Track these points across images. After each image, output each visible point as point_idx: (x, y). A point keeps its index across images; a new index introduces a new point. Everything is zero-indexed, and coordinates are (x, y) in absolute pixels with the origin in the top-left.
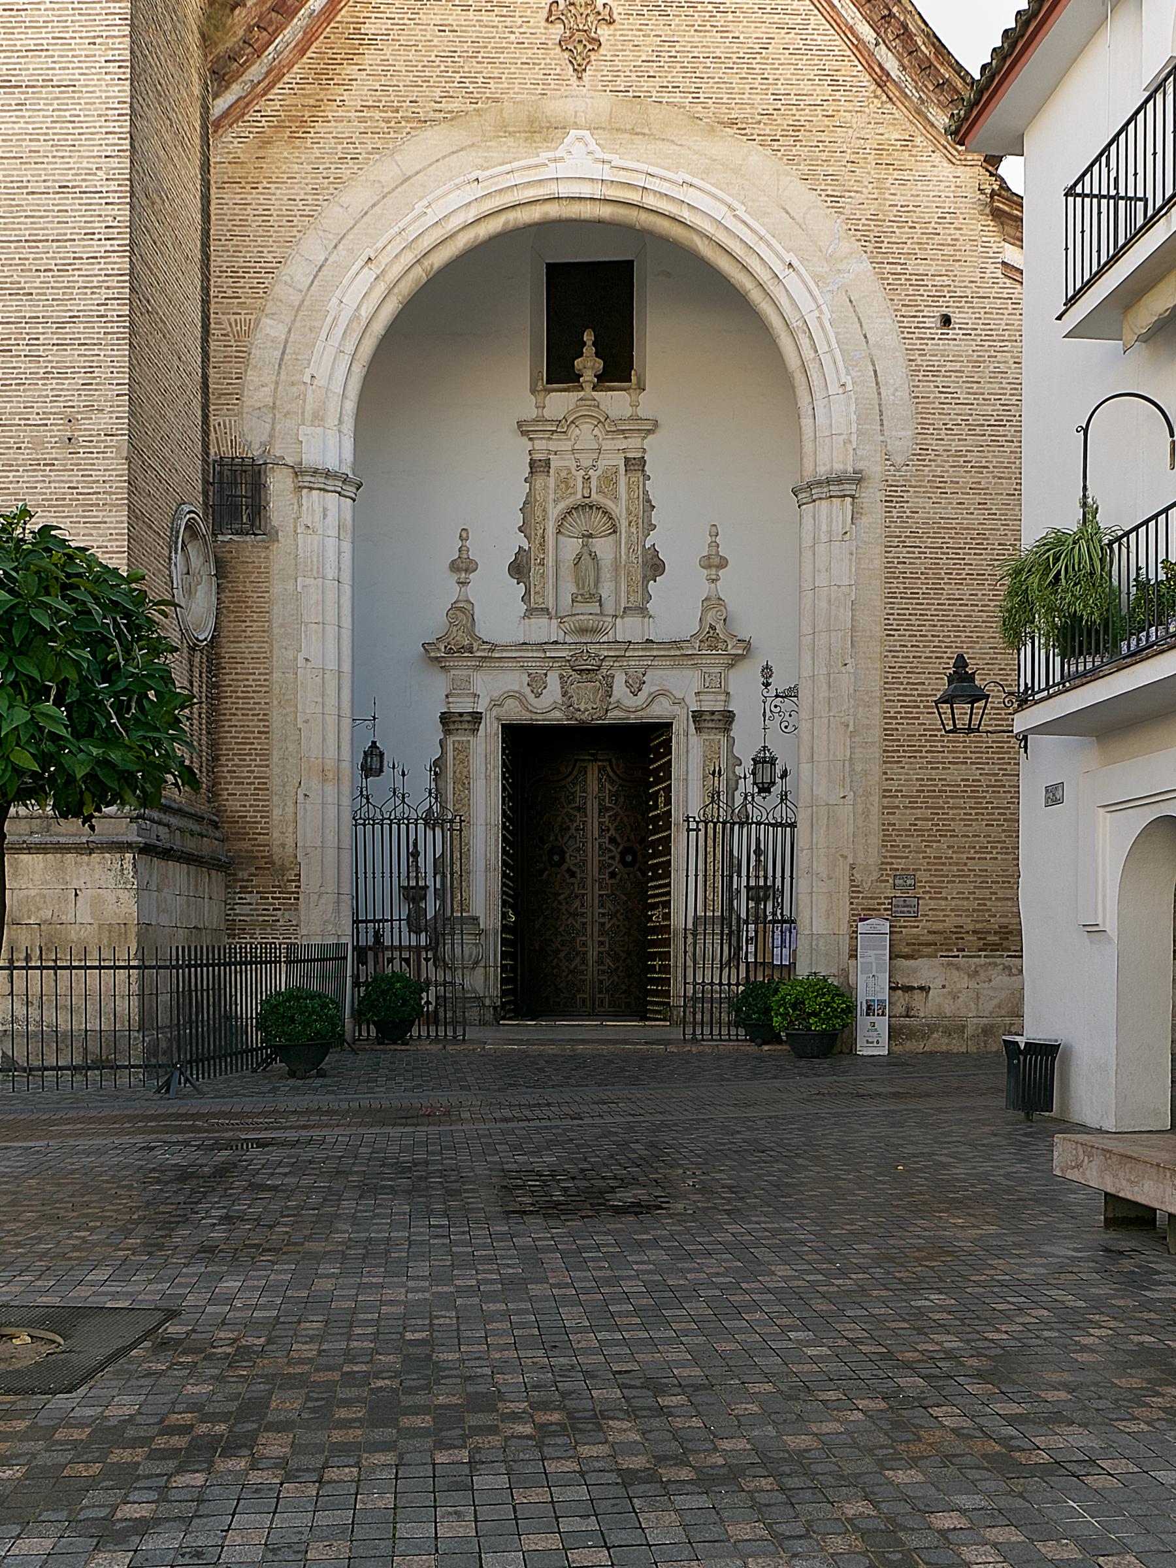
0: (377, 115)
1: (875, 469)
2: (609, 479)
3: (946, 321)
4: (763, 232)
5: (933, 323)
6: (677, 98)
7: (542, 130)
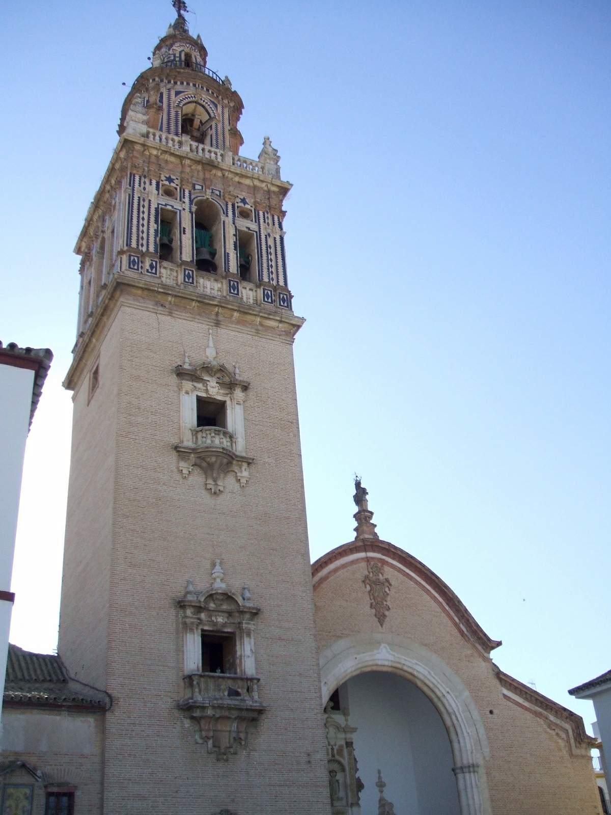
0: (324, 633)
1: (481, 762)
2: (340, 752)
3: (491, 712)
4: (439, 681)
5: (488, 713)
6: (409, 636)
7: (374, 644)
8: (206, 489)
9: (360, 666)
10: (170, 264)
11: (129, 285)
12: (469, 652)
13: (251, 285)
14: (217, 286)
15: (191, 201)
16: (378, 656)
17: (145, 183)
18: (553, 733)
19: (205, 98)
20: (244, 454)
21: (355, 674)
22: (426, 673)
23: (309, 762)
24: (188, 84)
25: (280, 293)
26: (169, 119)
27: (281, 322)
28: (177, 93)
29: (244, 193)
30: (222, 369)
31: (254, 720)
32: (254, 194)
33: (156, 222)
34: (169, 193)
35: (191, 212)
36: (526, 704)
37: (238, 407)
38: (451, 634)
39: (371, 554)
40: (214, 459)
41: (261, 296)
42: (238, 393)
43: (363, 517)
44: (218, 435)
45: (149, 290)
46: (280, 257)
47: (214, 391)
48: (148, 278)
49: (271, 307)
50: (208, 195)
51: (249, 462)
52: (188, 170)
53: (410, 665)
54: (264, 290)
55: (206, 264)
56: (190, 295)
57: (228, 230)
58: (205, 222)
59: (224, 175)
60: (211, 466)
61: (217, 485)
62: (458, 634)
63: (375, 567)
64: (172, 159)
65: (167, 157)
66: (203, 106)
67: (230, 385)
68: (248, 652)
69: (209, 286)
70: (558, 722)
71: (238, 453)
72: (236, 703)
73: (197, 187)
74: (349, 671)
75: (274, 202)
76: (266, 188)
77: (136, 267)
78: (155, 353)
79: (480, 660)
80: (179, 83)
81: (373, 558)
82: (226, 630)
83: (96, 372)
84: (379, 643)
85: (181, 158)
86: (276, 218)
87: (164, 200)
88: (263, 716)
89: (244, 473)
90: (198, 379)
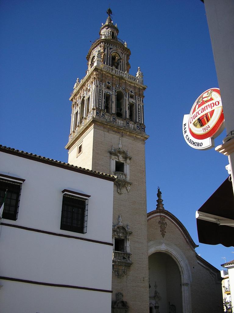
3: (194, 268)
7: (161, 243)
8: (117, 192)
9: (156, 250)
10: (108, 114)
11: (96, 121)
12: (189, 248)
13: (133, 123)
14: (122, 122)
15: (115, 91)
16: (162, 247)
17: (101, 84)
18: (211, 275)
19: (119, 51)
20: (129, 181)
21: (154, 252)
22: (175, 254)
23: (144, 280)
24: (114, 46)
25: (142, 126)
26: (107, 59)
27: (142, 136)
28: (110, 49)
29: (132, 89)
30: (124, 152)
31: (129, 266)
32: (135, 89)
33: (104, 99)
34: (108, 88)
35: (115, 95)
36: (204, 266)
37: (128, 165)
38: (184, 242)
39: (161, 214)
40: (120, 183)
41: (136, 127)
42: (128, 160)
43: (159, 201)
44: (122, 175)
45: (102, 123)
46: (142, 113)
47: (121, 160)
48: (102, 119)
49: (139, 131)
50: (121, 89)
51: (130, 184)
52: (114, 79)
53: (171, 251)
54: (137, 124)
55: (119, 114)
56: (115, 126)
57: (127, 101)
58: (119, 97)
59: (125, 82)
60: (119, 185)
61: (121, 191)
62: (186, 242)
63: (163, 218)
64: (109, 75)
65: (108, 74)
66: (119, 54)
67: (126, 158)
68: (128, 246)
69: (120, 122)
70: (213, 272)
71: (127, 181)
72: (125, 261)
73: (117, 86)
74: (153, 251)
75: (141, 92)
76: (138, 87)
77: (98, 115)
78: (103, 145)
79: (192, 251)
80: (111, 45)
81: (162, 215)
82: (122, 238)
83: (80, 148)
84: (162, 243)
85: (113, 75)
86: (141, 98)
87: (107, 90)
88: (131, 266)
89: (129, 188)
90: (115, 155)
